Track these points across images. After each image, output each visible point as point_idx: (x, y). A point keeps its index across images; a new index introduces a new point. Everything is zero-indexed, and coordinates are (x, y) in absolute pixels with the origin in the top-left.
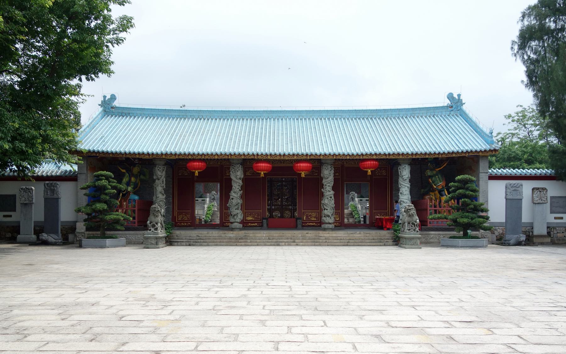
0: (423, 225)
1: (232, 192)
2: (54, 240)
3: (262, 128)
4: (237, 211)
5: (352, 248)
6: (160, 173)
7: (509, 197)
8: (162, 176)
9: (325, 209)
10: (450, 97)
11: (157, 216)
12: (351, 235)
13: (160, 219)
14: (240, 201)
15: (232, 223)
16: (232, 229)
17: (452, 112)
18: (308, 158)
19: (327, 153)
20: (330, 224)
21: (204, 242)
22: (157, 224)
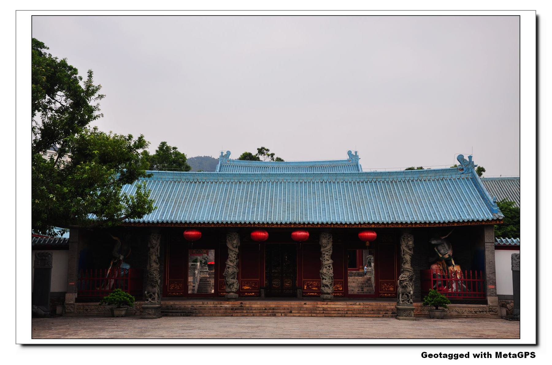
0: (422, 293)
1: (228, 260)
2: (43, 313)
3: (259, 194)
4: (233, 280)
5: (350, 319)
6: (155, 242)
7: (514, 269)
8: (156, 244)
9: (323, 279)
10: (460, 158)
11: (155, 287)
12: (350, 306)
13: (157, 289)
14: (331, 261)
15: (227, 292)
16: (228, 299)
17: (463, 176)
18: (306, 226)
19: (325, 222)
20: (329, 294)
21: (200, 313)
22: (154, 294)
